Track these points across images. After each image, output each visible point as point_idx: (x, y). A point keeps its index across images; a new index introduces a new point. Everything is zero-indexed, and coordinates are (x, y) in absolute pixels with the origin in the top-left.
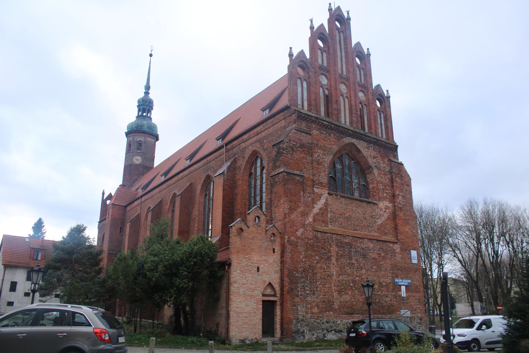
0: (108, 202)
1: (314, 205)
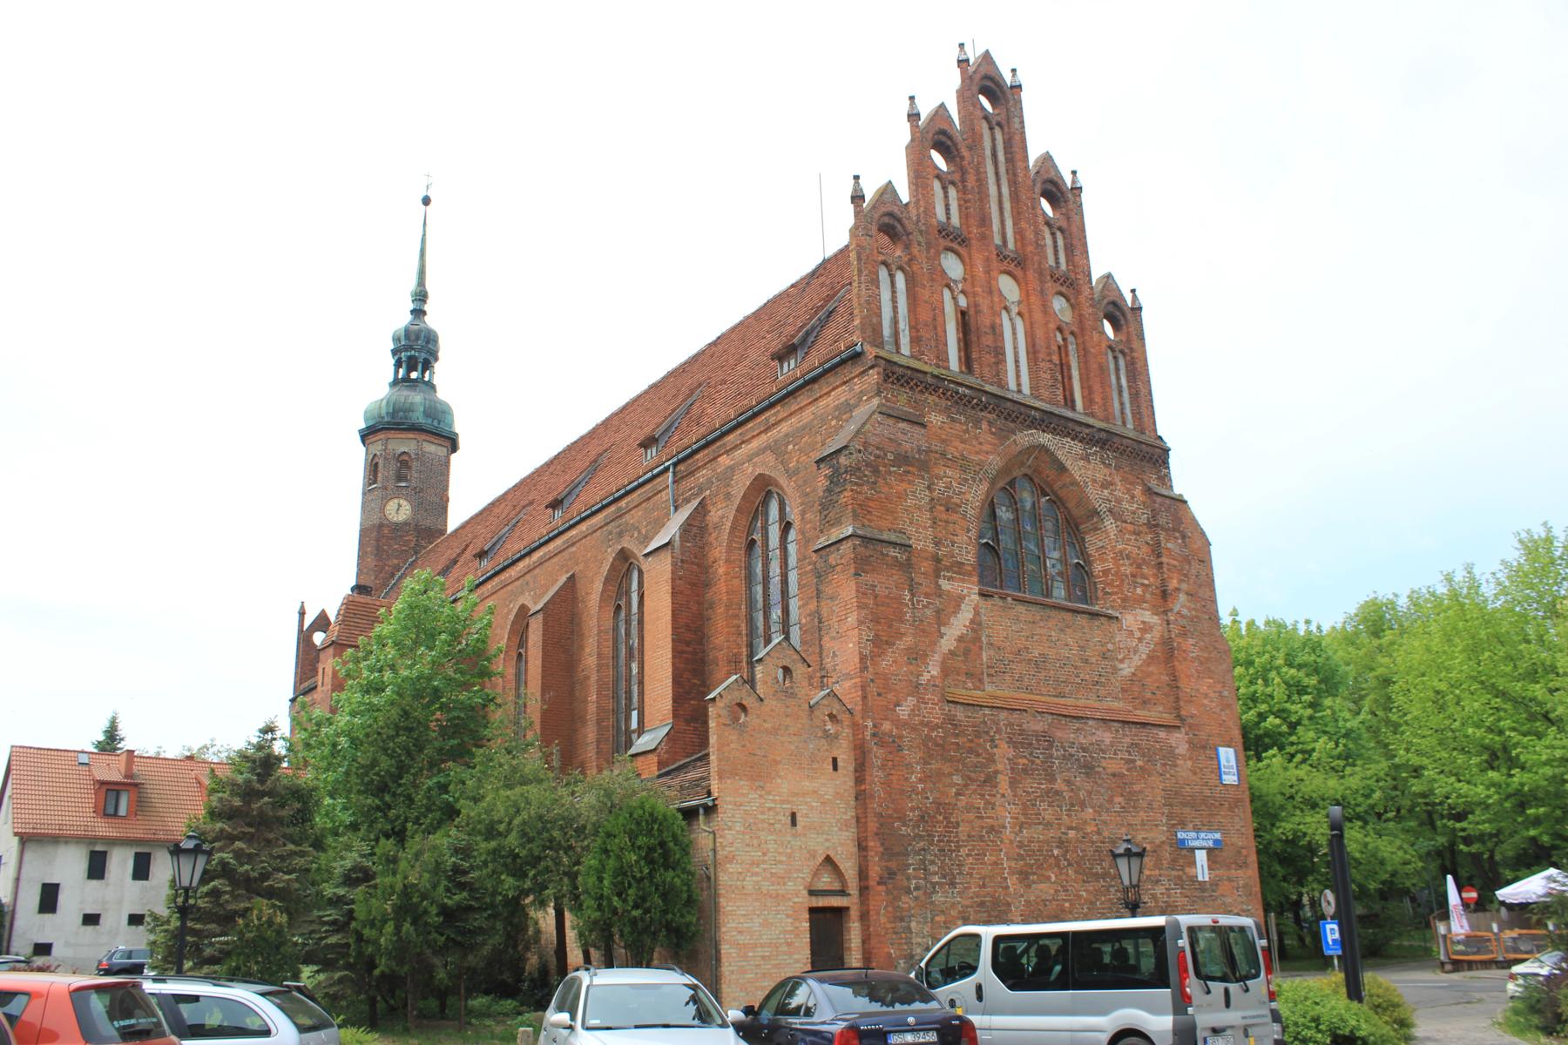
0: (318, 638)
1: (943, 629)
